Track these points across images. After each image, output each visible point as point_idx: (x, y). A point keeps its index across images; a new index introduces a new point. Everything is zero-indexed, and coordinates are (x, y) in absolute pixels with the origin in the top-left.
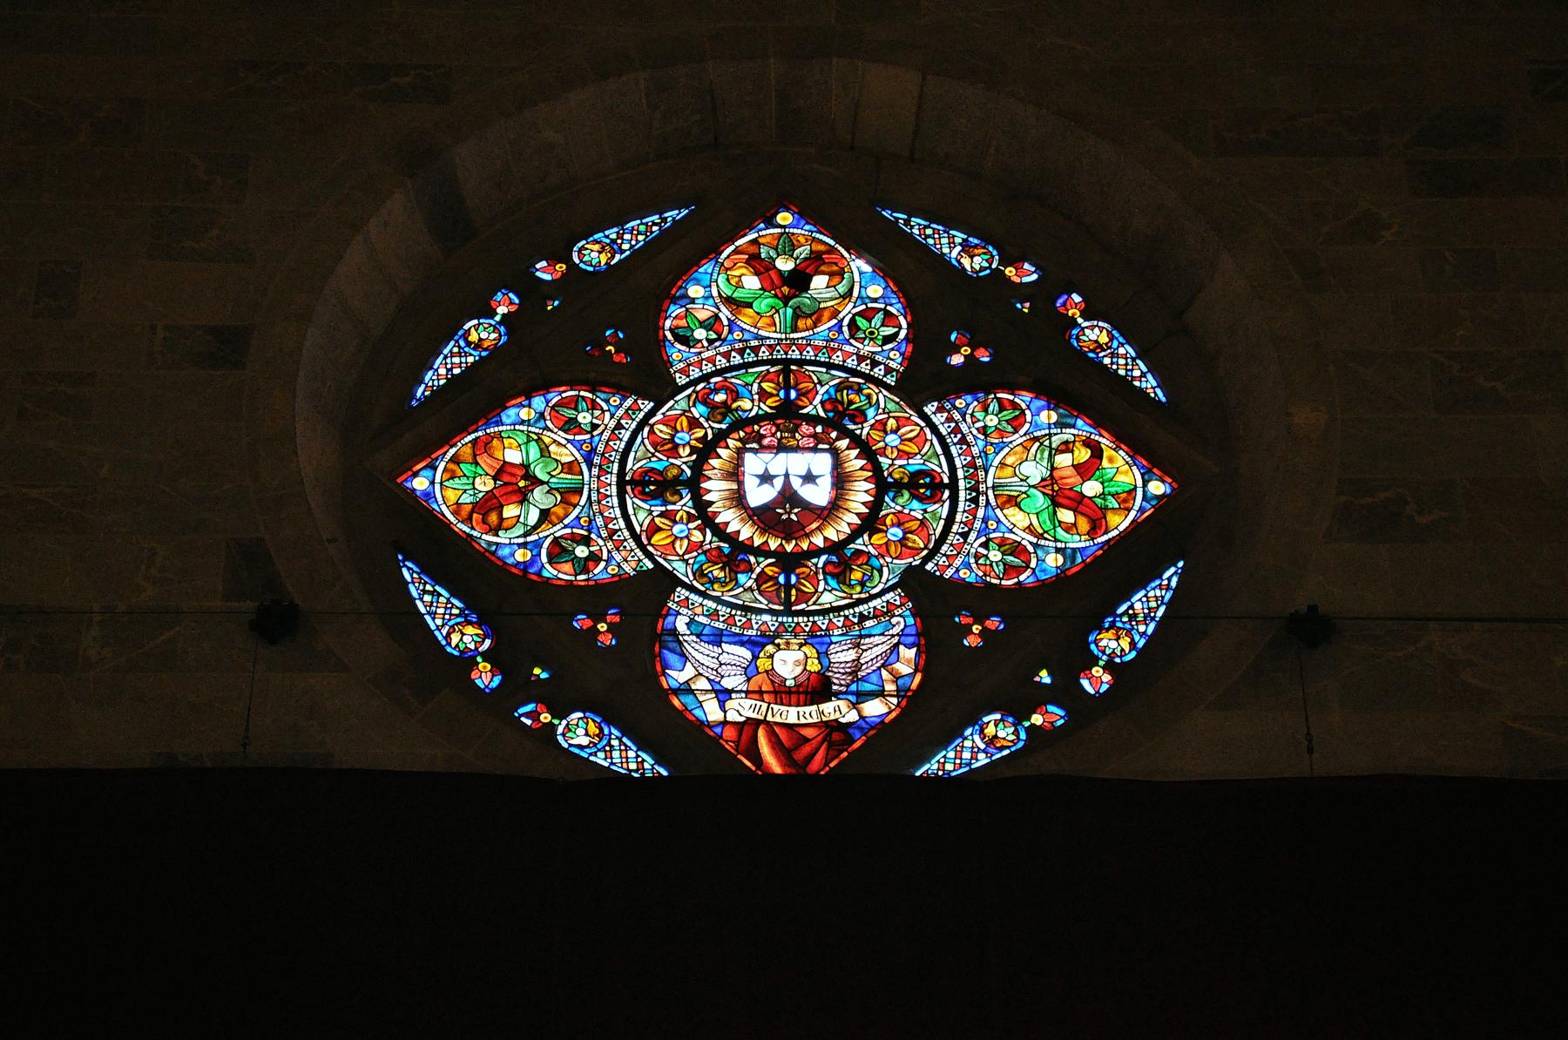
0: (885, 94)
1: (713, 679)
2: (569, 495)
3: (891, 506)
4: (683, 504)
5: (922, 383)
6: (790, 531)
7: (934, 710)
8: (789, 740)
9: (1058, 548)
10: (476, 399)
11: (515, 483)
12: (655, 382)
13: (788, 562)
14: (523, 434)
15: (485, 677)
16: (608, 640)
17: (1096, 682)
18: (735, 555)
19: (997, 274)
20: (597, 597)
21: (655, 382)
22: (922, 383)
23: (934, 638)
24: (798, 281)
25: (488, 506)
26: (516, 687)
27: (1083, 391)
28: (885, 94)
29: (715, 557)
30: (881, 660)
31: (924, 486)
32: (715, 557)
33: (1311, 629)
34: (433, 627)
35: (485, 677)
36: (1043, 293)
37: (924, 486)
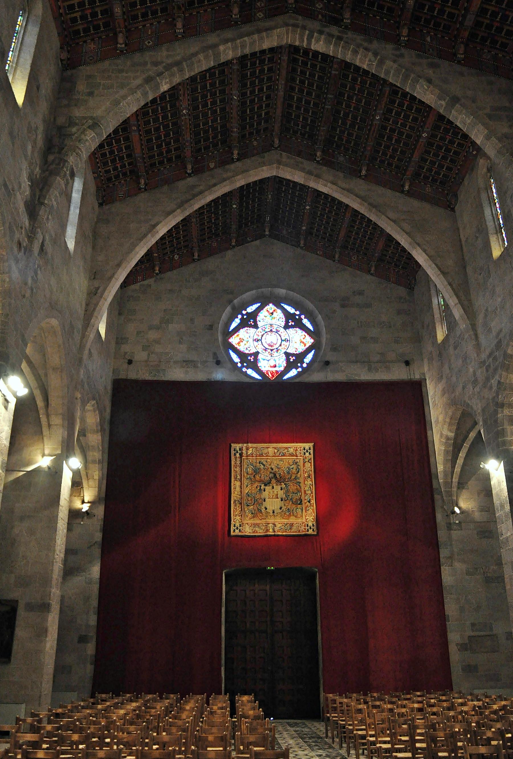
0: (282, 292)
1: (264, 365)
2: (247, 342)
3: (283, 339)
4: (260, 342)
5: (287, 327)
6: (272, 346)
7: (287, 369)
8: (272, 373)
9: (301, 349)
10: (237, 329)
11: (241, 340)
12: (256, 326)
13: (272, 350)
14: (243, 333)
15: (239, 365)
16: (252, 360)
17: (305, 365)
18: (266, 350)
19: (298, 372)
20: (251, 355)
21: (256, 326)
22: (287, 327)
23: (288, 360)
24: (272, 314)
25: (239, 343)
26: (243, 366)
27: (303, 328)
28: (282, 292)
29: (264, 349)
30: (281, 363)
31: (287, 340)
32: (264, 349)
33: (327, 363)
34: (250, 445)
35: (239, 365)
36: (299, 315)
37: (287, 340)
